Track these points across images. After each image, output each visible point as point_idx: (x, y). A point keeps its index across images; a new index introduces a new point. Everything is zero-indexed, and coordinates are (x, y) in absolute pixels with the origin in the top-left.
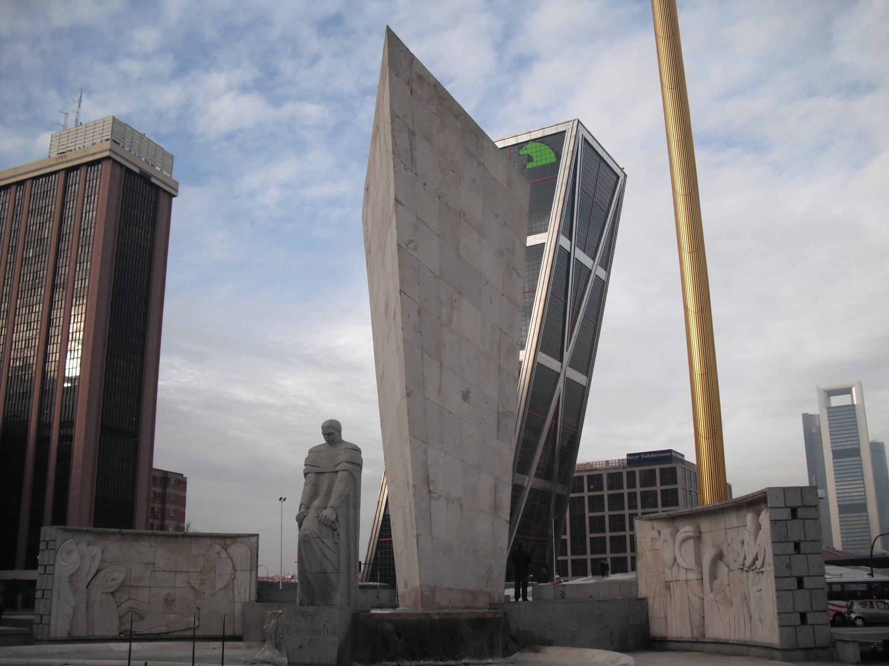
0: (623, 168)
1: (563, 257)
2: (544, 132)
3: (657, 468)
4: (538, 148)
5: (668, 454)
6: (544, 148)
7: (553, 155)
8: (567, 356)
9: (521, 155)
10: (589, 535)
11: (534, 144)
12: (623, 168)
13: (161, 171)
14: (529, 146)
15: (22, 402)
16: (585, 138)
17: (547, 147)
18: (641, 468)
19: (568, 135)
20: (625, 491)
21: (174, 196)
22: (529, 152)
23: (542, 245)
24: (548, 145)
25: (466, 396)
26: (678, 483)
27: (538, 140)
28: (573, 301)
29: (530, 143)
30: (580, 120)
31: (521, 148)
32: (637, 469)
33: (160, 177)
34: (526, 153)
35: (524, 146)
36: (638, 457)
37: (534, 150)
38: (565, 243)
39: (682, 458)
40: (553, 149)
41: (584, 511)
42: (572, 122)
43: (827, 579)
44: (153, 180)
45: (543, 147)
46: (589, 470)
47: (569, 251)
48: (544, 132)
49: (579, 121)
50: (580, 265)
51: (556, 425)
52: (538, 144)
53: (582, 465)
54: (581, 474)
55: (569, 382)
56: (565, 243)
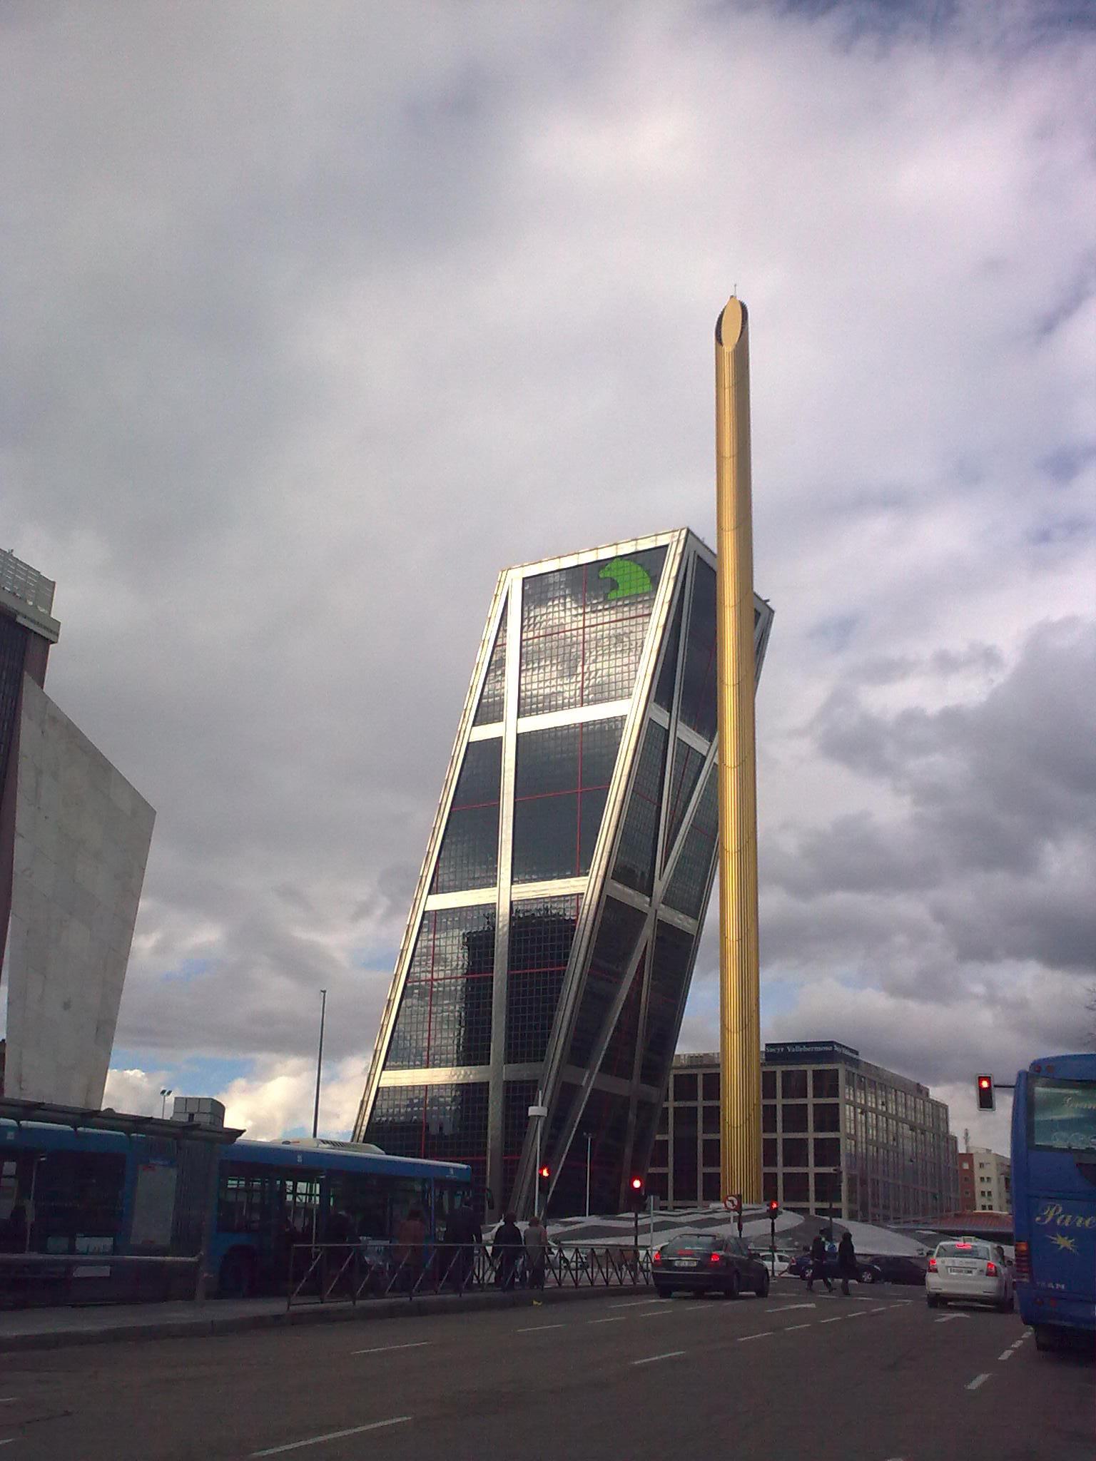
0: (768, 601)
1: (653, 737)
2: (636, 545)
3: (810, 1069)
4: (627, 570)
5: (826, 1048)
6: (635, 570)
7: (648, 581)
8: (659, 887)
9: (602, 579)
10: (669, 1170)
11: (621, 563)
12: (768, 601)
13: (35, 606)
14: (613, 565)
15: (461, 728)
16: (698, 556)
17: (639, 568)
18: (784, 1068)
19: (671, 553)
20: (700, 1103)
21: (53, 643)
22: (613, 574)
23: (623, 718)
24: (641, 565)
25: (66, 1006)
26: (840, 1095)
27: (627, 558)
28: (672, 804)
29: (615, 560)
30: (690, 528)
31: (602, 567)
32: (779, 1070)
33: (31, 615)
34: (608, 575)
35: (607, 565)
36: (782, 1049)
37: (621, 572)
38: (662, 718)
39: (855, 1056)
40: (648, 572)
41: (696, 1131)
42: (679, 532)
43: (857, 1258)
44: (20, 620)
45: (634, 567)
46: (708, 1066)
47: (667, 728)
48: (636, 545)
49: (688, 531)
50: (683, 747)
51: (640, 994)
52: (627, 563)
53: (697, 1057)
54: (694, 1071)
55: (664, 928)
56: (662, 718)
